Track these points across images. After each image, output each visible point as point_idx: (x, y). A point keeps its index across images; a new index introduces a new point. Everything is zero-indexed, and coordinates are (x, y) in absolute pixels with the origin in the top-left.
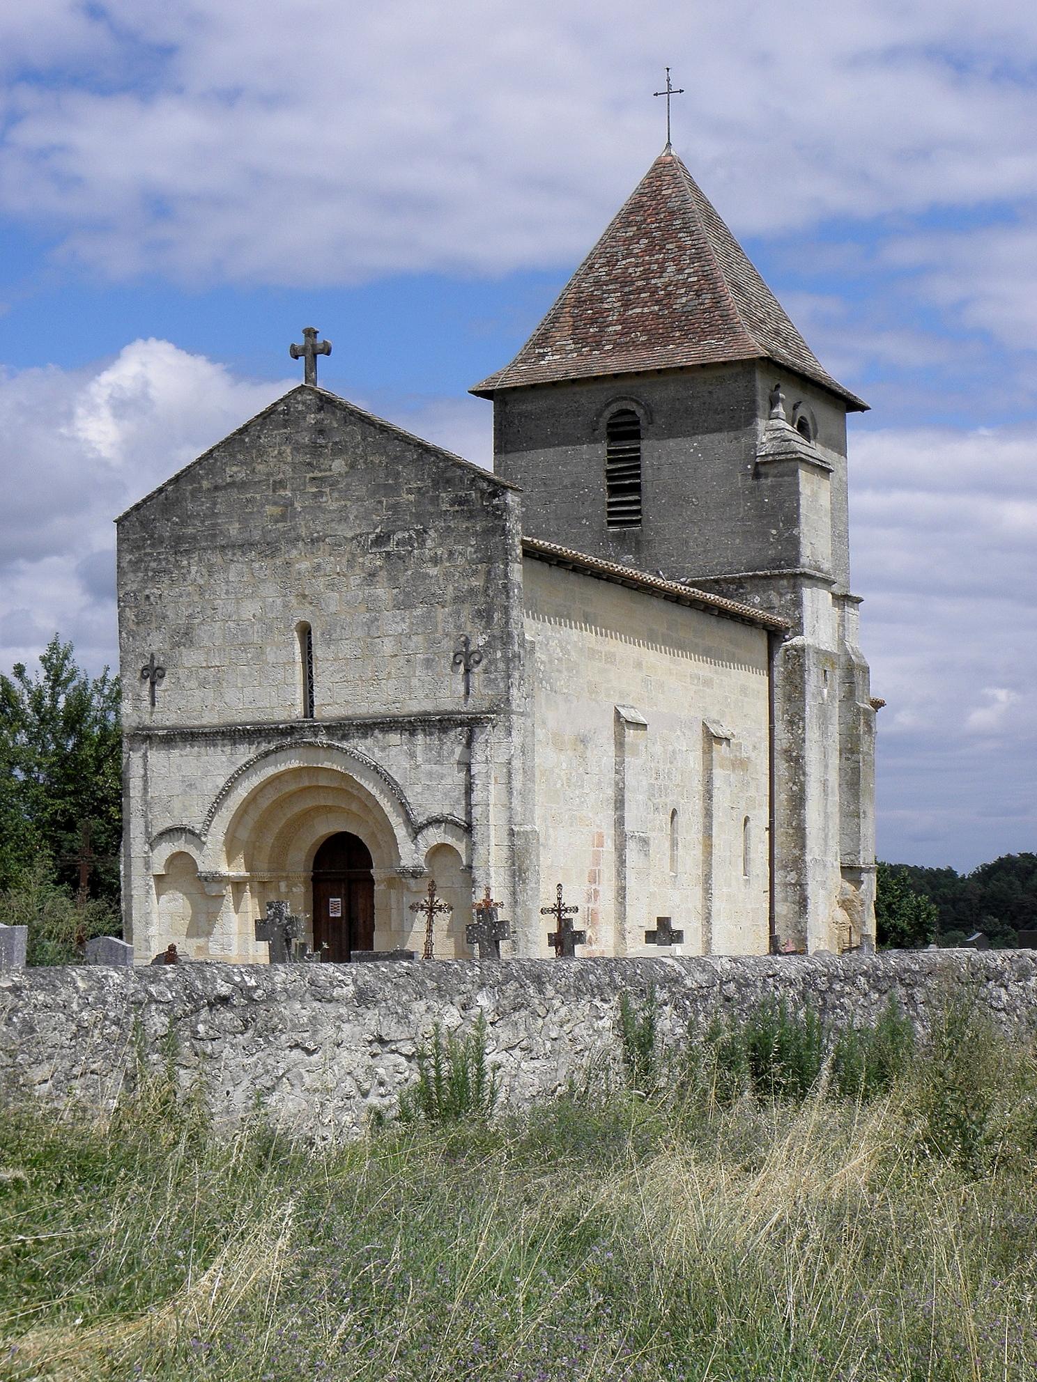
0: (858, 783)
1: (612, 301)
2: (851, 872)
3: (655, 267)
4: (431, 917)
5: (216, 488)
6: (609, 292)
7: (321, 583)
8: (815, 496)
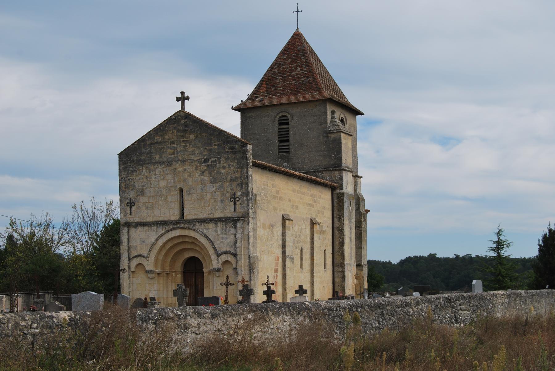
0: (361, 238)
1: (279, 79)
2: (359, 266)
3: (293, 68)
4: (227, 287)
5: (152, 144)
6: (278, 76)
7: (186, 175)
8: (346, 144)
